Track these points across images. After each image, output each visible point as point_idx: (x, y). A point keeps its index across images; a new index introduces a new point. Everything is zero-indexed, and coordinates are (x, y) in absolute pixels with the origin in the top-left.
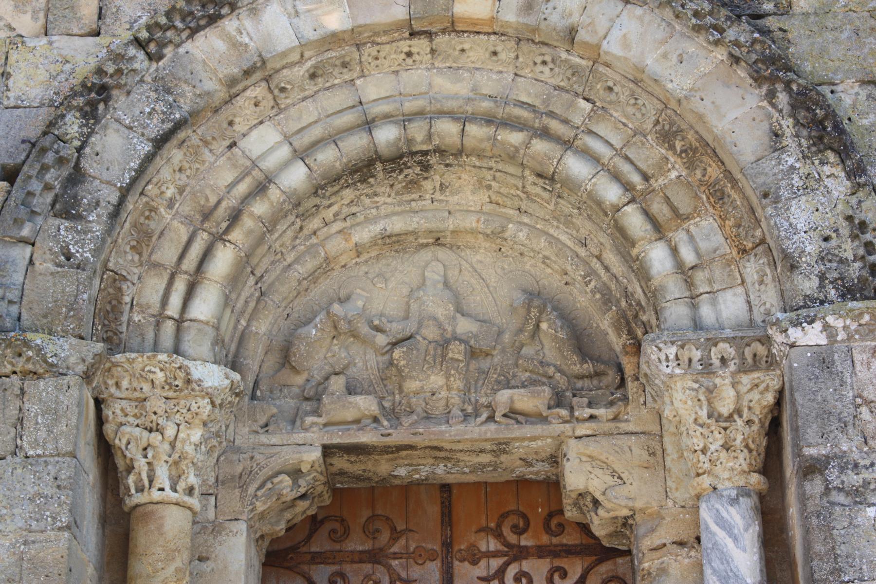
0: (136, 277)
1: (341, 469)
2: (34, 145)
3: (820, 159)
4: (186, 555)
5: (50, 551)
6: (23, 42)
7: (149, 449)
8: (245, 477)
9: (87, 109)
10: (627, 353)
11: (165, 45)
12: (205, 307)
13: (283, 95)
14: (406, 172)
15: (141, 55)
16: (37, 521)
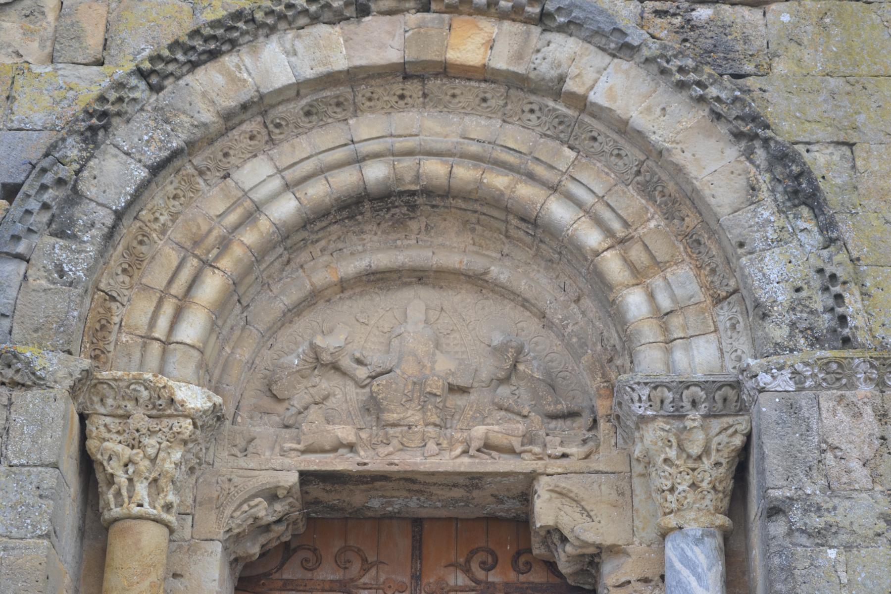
0: (126, 299)
1: (316, 498)
2: (34, 167)
3: (794, 214)
4: (161, 572)
5: (29, 558)
6: (29, 69)
7: (130, 466)
8: (222, 499)
9: (88, 134)
10: (600, 396)
11: (166, 77)
12: (191, 330)
13: (277, 131)
14: (393, 211)
15: (143, 85)
16: (18, 528)
